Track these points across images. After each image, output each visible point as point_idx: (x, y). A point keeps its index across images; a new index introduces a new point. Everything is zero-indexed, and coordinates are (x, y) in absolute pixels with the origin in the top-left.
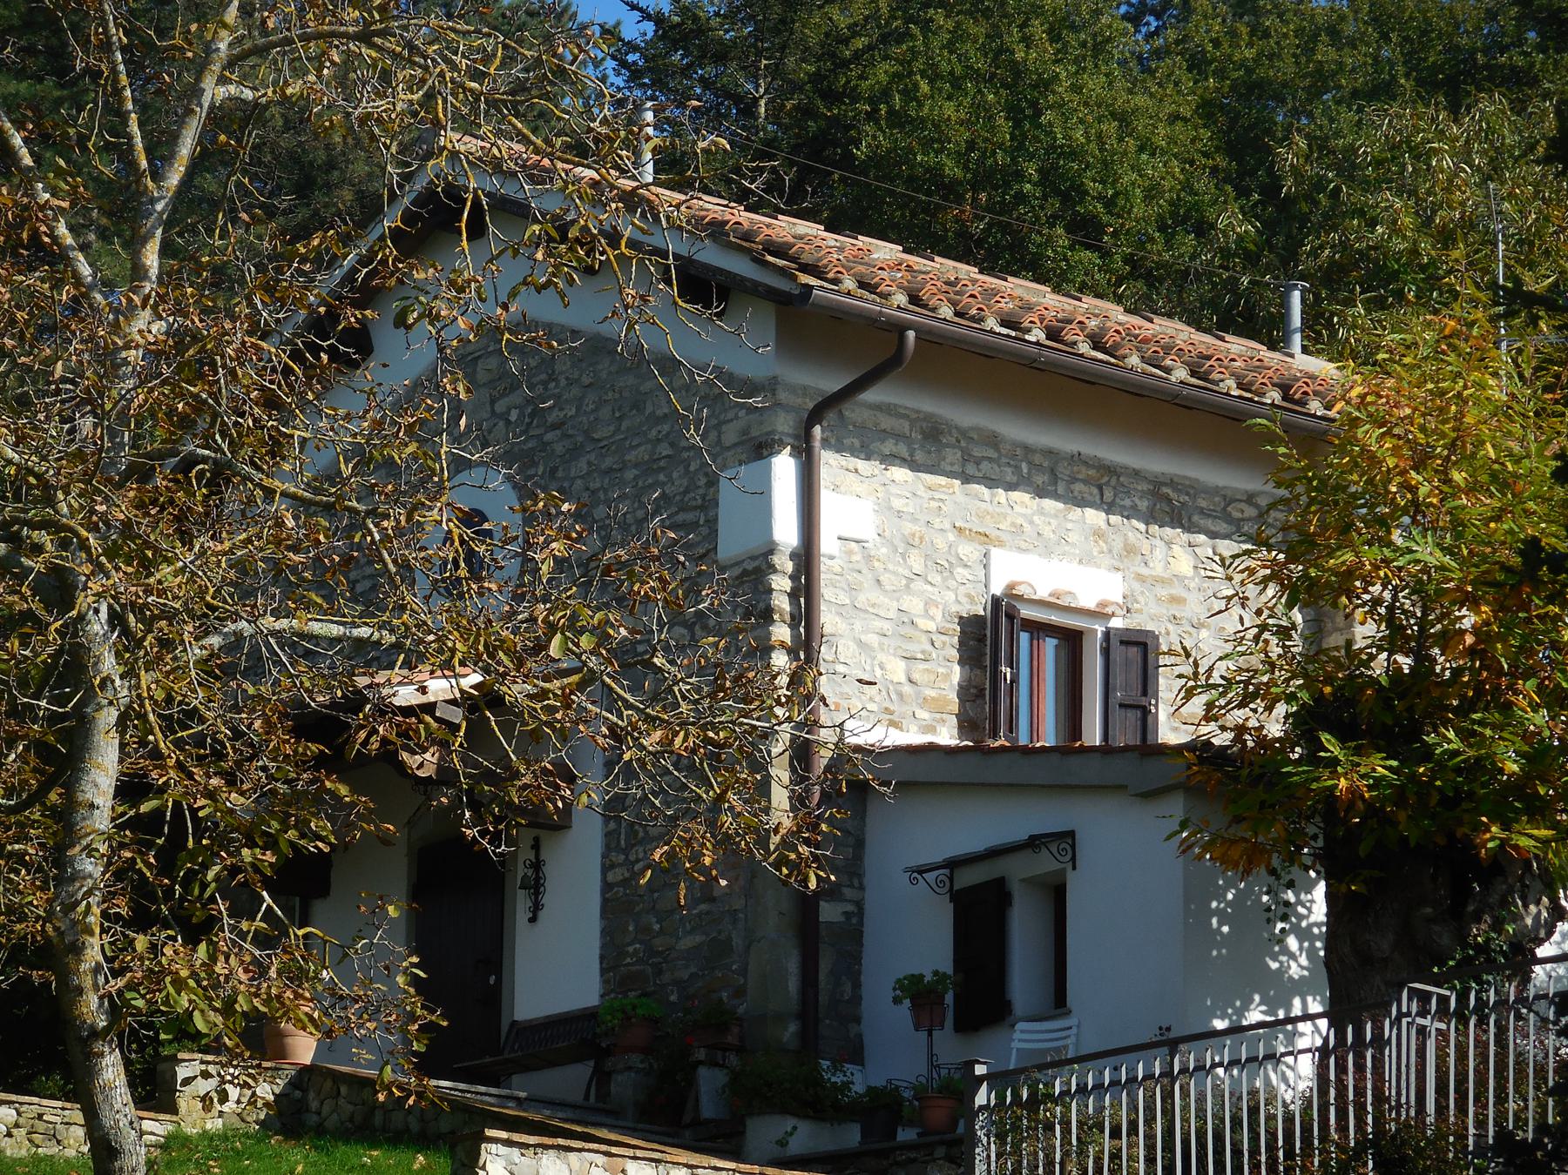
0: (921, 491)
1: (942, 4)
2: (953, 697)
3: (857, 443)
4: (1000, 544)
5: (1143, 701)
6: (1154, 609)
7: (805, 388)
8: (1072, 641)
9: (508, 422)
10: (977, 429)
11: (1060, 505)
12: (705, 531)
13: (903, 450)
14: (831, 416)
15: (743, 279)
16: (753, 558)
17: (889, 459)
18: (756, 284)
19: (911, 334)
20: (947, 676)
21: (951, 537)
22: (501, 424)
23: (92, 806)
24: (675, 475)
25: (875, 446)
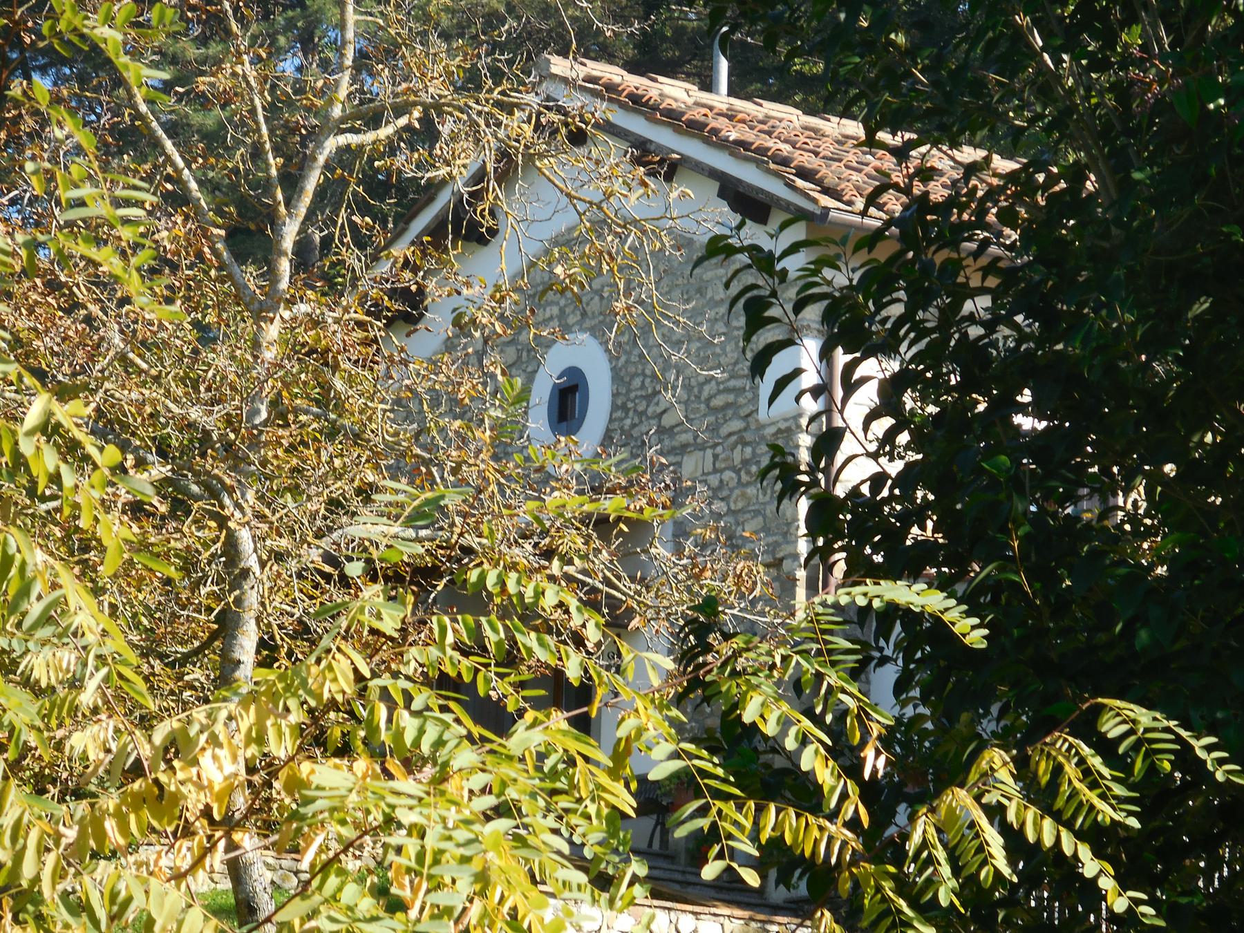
9: (602, 297)
12: (749, 395)
15: (779, 199)
16: (786, 420)
18: (789, 204)
22: (597, 298)
23: (239, 662)
24: (728, 349)
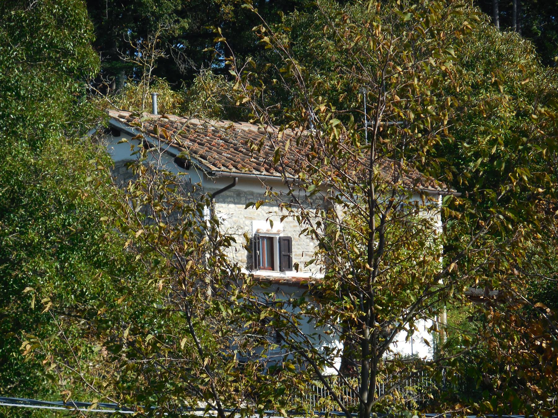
0: (237, 209)
1: (392, 417)
2: (246, 259)
3: (222, 200)
4: (255, 219)
5: (289, 254)
6: (290, 229)
7: (210, 188)
8: (271, 240)
10: (249, 191)
11: (268, 207)
13: (232, 200)
14: (217, 196)
17: (229, 203)
19: (237, 179)
20: (244, 254)
21: (244, 219)
25: (226, 200)
